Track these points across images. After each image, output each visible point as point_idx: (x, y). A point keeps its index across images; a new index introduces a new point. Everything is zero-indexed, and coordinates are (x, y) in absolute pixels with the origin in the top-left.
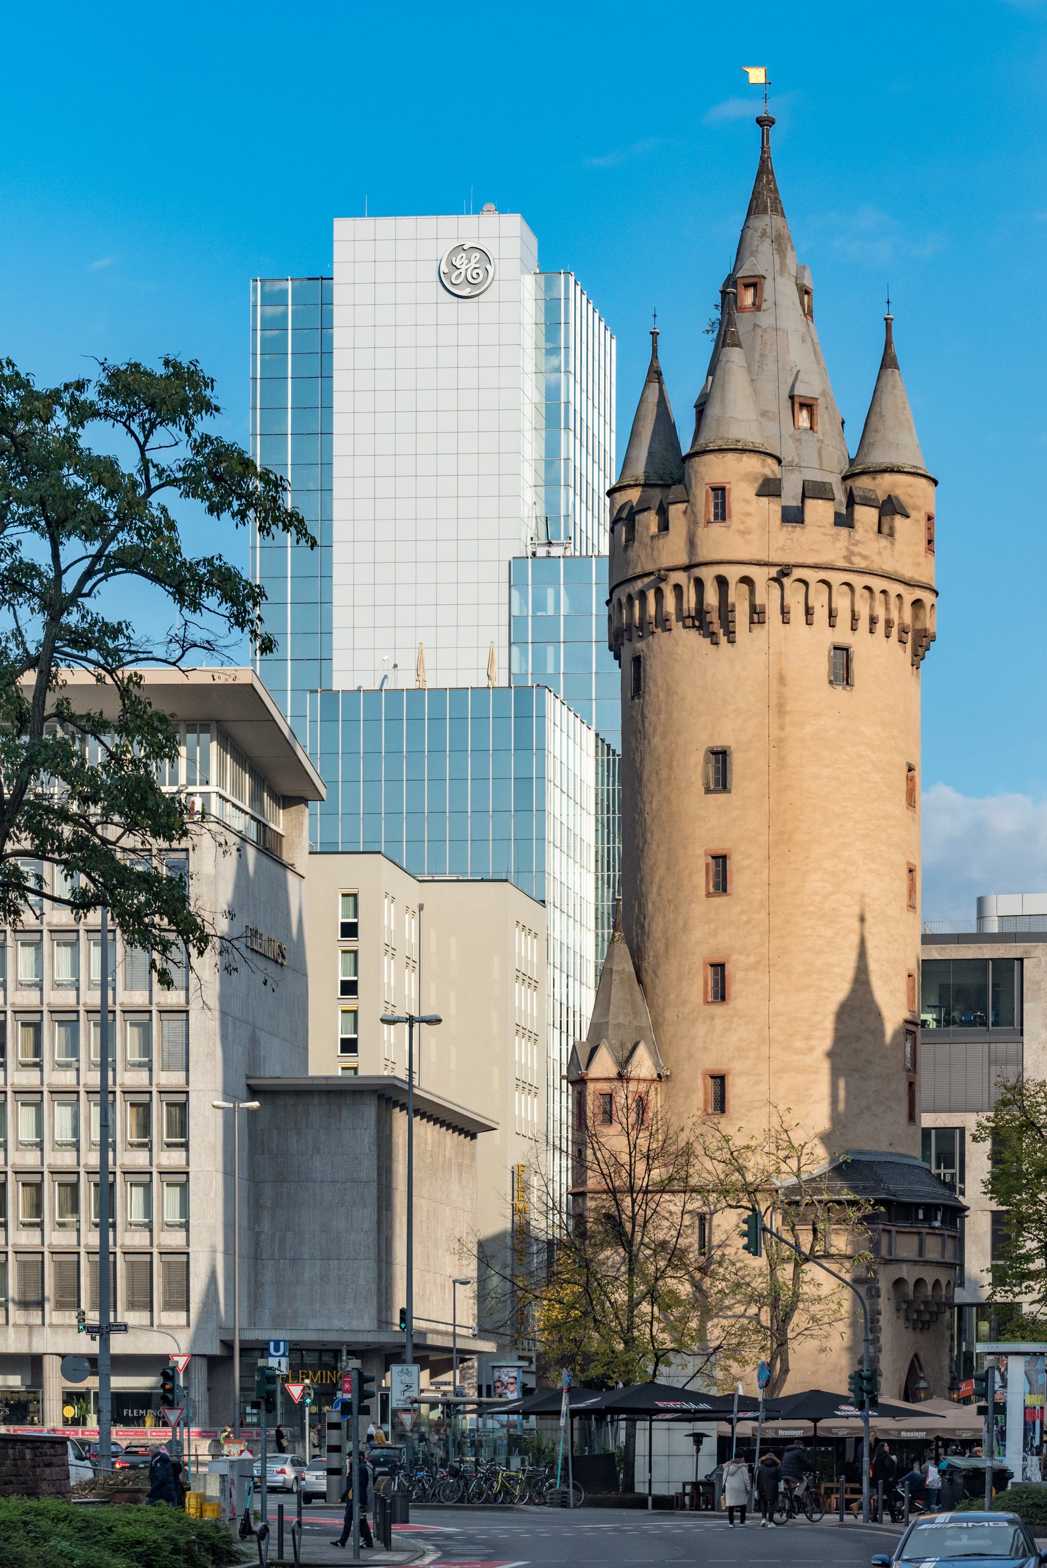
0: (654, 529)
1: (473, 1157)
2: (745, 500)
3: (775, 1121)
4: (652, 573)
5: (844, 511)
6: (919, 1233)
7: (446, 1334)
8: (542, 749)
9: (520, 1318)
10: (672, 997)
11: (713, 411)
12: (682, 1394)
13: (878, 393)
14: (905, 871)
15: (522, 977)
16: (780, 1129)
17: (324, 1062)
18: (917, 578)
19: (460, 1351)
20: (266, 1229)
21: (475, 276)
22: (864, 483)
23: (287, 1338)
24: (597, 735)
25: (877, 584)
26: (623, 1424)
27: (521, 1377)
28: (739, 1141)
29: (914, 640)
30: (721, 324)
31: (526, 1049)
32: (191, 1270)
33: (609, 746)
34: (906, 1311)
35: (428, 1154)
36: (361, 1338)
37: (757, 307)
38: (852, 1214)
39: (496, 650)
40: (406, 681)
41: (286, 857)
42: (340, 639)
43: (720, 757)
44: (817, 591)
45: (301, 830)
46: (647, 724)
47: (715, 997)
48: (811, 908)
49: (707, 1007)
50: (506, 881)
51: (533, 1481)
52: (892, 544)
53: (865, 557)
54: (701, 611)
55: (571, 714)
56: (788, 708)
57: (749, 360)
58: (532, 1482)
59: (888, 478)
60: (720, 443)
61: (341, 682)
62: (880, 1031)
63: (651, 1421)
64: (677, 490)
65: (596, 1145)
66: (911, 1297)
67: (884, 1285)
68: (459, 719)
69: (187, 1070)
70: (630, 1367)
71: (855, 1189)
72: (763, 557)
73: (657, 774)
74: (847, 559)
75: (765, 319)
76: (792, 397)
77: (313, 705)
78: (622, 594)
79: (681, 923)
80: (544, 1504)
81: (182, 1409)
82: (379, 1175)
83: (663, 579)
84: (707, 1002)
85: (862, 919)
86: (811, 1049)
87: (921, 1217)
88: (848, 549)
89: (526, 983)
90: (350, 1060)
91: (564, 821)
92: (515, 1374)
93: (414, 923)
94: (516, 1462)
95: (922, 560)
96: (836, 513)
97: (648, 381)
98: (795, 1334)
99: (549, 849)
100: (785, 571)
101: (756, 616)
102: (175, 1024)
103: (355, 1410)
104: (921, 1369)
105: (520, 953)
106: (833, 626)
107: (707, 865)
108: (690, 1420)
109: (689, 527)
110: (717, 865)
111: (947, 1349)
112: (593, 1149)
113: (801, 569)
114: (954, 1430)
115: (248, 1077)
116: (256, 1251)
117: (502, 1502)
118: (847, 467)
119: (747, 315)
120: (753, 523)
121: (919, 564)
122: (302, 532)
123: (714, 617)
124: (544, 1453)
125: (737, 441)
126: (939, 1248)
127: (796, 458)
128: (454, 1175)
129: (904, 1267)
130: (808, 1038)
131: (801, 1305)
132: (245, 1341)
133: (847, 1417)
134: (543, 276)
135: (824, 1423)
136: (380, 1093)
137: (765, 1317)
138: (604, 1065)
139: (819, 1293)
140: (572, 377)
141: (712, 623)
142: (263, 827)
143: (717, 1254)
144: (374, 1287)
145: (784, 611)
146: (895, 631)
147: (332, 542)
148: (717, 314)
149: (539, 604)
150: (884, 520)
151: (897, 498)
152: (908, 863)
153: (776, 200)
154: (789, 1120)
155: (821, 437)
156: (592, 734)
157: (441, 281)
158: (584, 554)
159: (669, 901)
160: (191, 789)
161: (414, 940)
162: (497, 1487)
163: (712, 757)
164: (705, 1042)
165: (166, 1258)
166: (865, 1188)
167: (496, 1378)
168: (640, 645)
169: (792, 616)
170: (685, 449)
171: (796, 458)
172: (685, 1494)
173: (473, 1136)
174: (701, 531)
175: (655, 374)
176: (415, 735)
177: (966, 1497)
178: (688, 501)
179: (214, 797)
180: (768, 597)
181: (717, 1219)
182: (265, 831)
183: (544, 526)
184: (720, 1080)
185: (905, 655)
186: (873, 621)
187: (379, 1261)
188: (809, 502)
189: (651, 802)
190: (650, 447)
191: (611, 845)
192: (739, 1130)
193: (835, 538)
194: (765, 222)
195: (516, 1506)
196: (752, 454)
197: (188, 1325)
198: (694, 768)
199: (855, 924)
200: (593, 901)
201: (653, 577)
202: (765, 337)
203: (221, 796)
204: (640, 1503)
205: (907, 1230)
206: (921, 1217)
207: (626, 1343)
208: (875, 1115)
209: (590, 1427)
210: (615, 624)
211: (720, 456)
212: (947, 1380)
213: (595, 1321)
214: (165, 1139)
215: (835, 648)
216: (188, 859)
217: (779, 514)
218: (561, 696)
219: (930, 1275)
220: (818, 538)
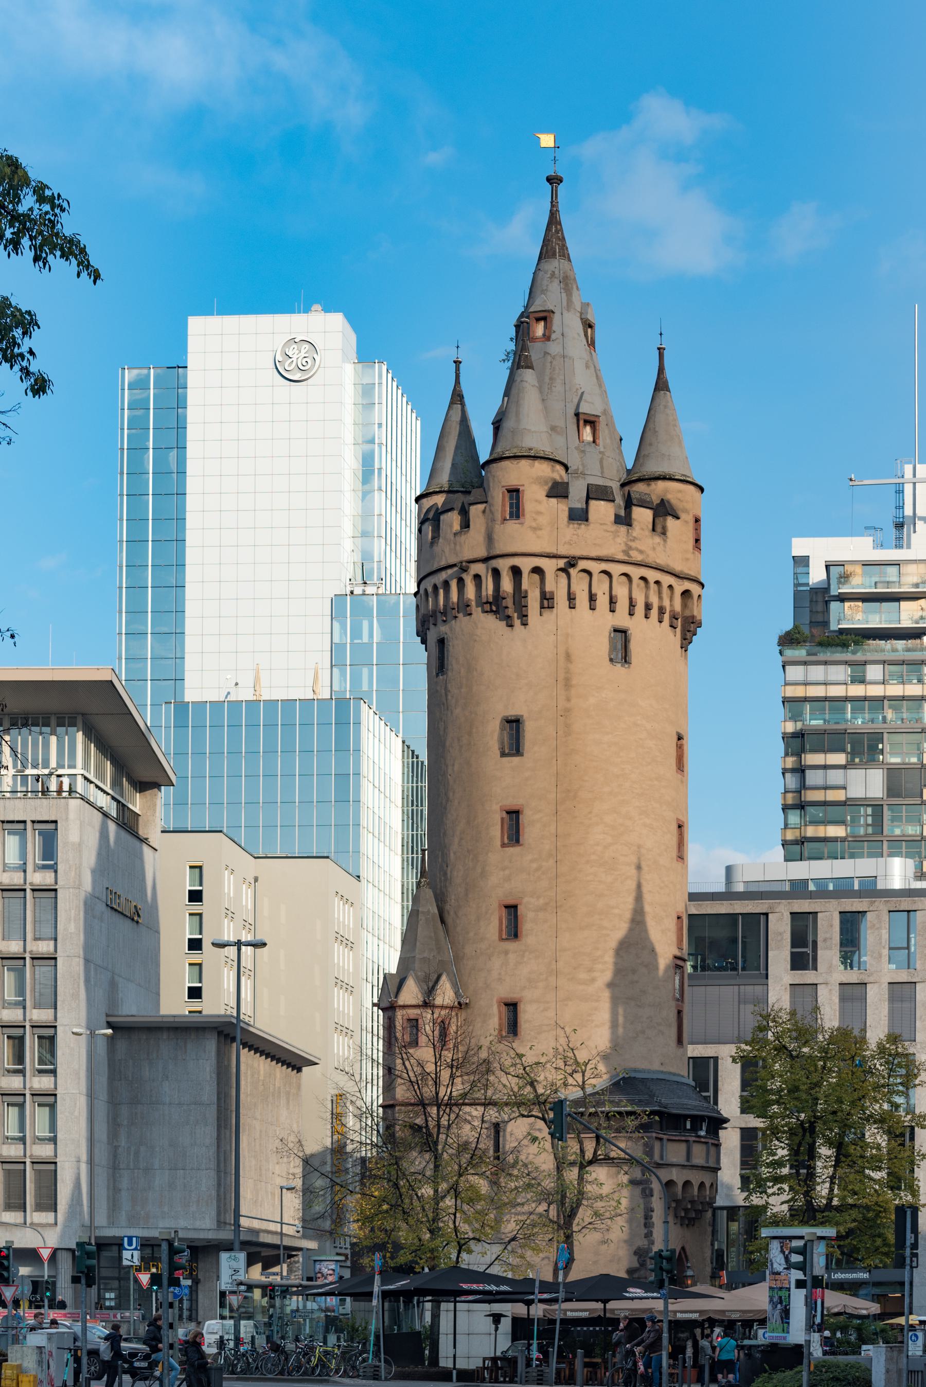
0: (457, 527)
1: (299, 1087)
2: (536, 501)
3: (563, 1041)
4: (454, 565)
5: (622, 513)
6: (687, 1141)
7: (275, 1233)
8: (358, 750)
9: (338, 1215)
10: (471, 934)
11: (508, 424)
12: (484, 1277)
13: (652, 412)
14: (675, 826)
15: (340, 938)
16: (566, 1048)
17: (174, 1004)
18: (686, 571)
19: (287, 1248)
20: (123, 1144)
21: (304, 364)
22: (640, 487)
23: (140, 1235)
24: (404, 742)
25: (652, 575)
26: (428, 1305)
27: (338, 1270)
28: (529, 1059)
29: (683, 626)
30: (515, 354)
31: (344, 955)
32: (58, 1177)
33: (413, 752)
34: (675, 1209)
35: (261, 1083)
36: (202, 1236)
37: (547, 337)
38: (631, 1123)
39: (320, 671)
40: (245, 694)
41: (142, 832)
42: (190, 662)
43: (514, 724)
44: (599, 581)
45: (155, 811)
46: (449, 697)
47: (509, 935)
48: (593, 857)
49: (502, 943)
50: (327, 857)
51: (348, 1356)
52: (665, 541)
53: (641, 552)
54: (498, 596)
55: (382, 723)
56: (574, 682)
57: (540, 380)
58: (346, 1356)
59: (661, 484)
60: (515, 451)
61: (190, 696)
62: (652, 965)
63: (455, 1302)
64: (476, 493)
65: (405, 1056)
66: (680, 1196)
67: (656, 1186)
68: (288, 726)
69: (56, 1008)
70: (435, 1254)
71: (632, 1102)
72: (552, 550)
73: (459, 740)
74: (626, 552)
75: (554, 348)
76: (577, 415)
77: (167, 715)
78: (428, 584)
79: (479, 871)
80: (358, 1376)
81: (17, 1286)
82: (219, 1099)
83: (464, 570)
84: (501, 939)
85: (639, 868)
86: (593, 980)
87: (688, 1127)
88: (626, 545)
89: (344, 943)
90: (195, 1005)
91: (376, 860)
92: (333, 1267)
93: (250, 892)
94: (332, 1339)
95: (690, 556)
96: (616, 515)
97: (452, 403)
98: (580, 1227)
99: (363, 833)
100: (572, 562)
101: (546, 602)
102: (44, 970)
103: (165, 1281)
104: (687, 1260)
105: (338, 919)
106: (613, 611)
107: (502, 819)
108: (489, 1302)
109: (487, 524)
110: (511, 819)
111: (709, 1243)
112: (402, 1059)
113: (585, 561)
114: (723, 1312)
115: (107, 1015)
116: (114, 1162)
117: (319, 1375)
118: (625, 476)
119: (538, 345)
120: (543, 520)
121: (687, 559)
122: (85, 264)
123: (509, 602)
124: (357, 1330)
125: (531, 449)
126: (704, 1154)
127: (580, 467)
128: (283, 1101)
129: (674, 1170)
130: (590, 970)
131: (585, 1202)
132: (100, 1237)
133: (632, 1299)
134: (360, 365)
135: (611, 1305)
136: (220, 1029)
137: (553, 1213)
138: (411, 993)
139: (601, 1192)
140: (384, 448)
141: (507, 608)
142: (121, 806)
143: (511, 1159)
144: (214, 1193)
145: (571, 598)
146: (666, 617)
147: (185, 583)
148: (512, 346)
149: (356, 632)
150: (657, 521)
151: (668, 502)
152: (678, 819)
153: (564, 247)
154: (575, 1041)
155: (602, 450)
156: (400, 741)
157: (277, 368)
158: (393, 592)
159: (468, 851)
160: (60, 772)
161: (250, 906)
162: (314, 1361)
163: (507, 725)
164: (500, 974)
165: (37, 1167)
166: (640, 1101)
167: (317, 1270)
168: (443, 629)
169: (578, 602)
170: (484, 457)
171: (580, 467)
172: (484, 1368)
173: (299, 1070)
174: (498, 528)
175: (457, 397)
176: (252, 738)
177: (765, 1371)
178: (486, 502)
179: (80, 779)
180: (556, 585)
181: (510, 1127)
182: (123, 810)
183: (360, 571)
184: (512, 1007)
185: (675, 639)
186: (648, 607)
187: (219, 1171)
188: (593, 504)
189: (453, 765)
190: (453, 459)
191: (420, 808)
192: (531, 1048)
193: (616, 534)
194: (553, 265)
195: (331, 1379)
196: (543, 461)
197: (56, 1224)
198: (491, 734)
199: (633, 871)
200: (400, 878)
201: (455, 569)
202: (554, 363)
203: (86, 778)
204: (445, 1376)
205: (677, 1138)
206: (688, 1127)
207: (431, 1232)
208: (648, 1038)
209: (399, 1308)
210: (422, 611)
211: (515, 462)
212: (708, 1270)
213: (404, 1213)
214: (37, 1066)
215: (616, 631)
216: (56, 829)
217: (566, 513)
218: (374, 707)
219: (696, 1178)
220: (600, 534)
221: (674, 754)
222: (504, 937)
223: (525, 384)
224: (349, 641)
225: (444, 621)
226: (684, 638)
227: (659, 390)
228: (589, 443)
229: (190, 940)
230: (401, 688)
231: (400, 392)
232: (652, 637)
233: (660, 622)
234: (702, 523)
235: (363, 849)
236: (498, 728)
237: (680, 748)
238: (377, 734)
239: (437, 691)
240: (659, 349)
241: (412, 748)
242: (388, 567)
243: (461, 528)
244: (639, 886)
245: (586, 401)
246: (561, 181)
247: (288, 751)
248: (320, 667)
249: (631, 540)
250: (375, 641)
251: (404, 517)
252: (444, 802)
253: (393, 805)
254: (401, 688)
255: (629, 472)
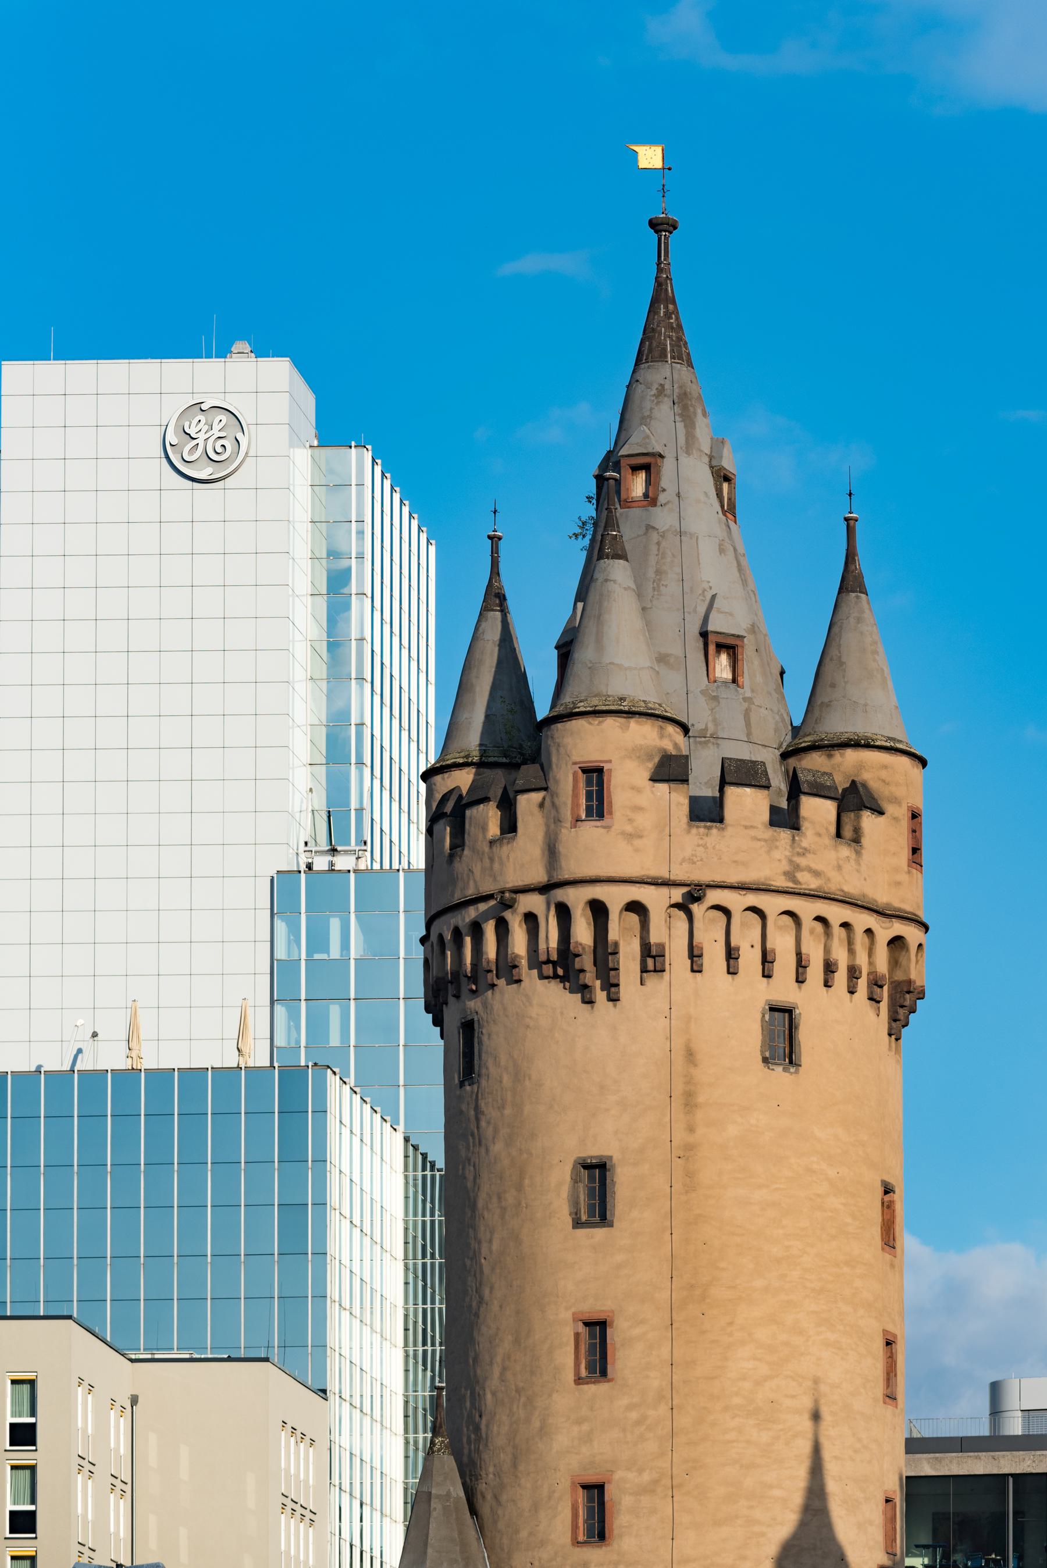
0: (494, 829)
2: (633, 788)
5: (784, 805)
8: (321, 1161)
10: (524, 1534)
11: (584, 655)
13: (835, 629)
14: (879, 1344)
15: (290, 1505)
18: (897, 904)
21: (219, 449)
22: (815, 761)
24: (407, 1140)
25: (836, 914)
29: (890, 997)
30: (596, 525)
33: (425, 1156)
37: (650, 499)
39: (250, 1012)
40: (110, 1057)
43: (597, 1173)
46: (483, 1124)
47: (590, 1534)
48: (737, 1400)
49: (578, 1550)
52: (858, 853)
53: (817, 874)
56: (701, 1099)
59: (851, 756)
60: (595, 701)
64: (528, 772)
68: (193, 1116)
72: (662, 873)
73: (499, 1198)
74: (790, 875)
75: (663, 518)
76: (704, 635)
78: (445, 927)
83: (508, 905)
84: (576, 1543)
85: (816, 1417)
88: (791, 862)
89: (297, 1514)
91: (356, 1360)
93: (124, 1424)
95: (903, 877)
97: (485, 609)
99: (333, 1311)
100: (694, 894)
101: (650, 962)
105: (288, 1470)
107: (577, 1336)
109: (547, 826)
110: (592, 1336)
118: (789, 738)
119: (635, 512)
120: (645, 821)
121: (898, 884)
123: (586, 962)
127: (711, 726)
141: (583, 972)
145: (694, 955)
146: (862, 984)
148: (590, 510)
149: (318, 940)
151: (864, 785)
153: (680, 342)
155: (748, 694)
157: (167, 457)
158: (386, 866)
159: (518, 1391)
161: (124, 1449)
163: (585, 1173)
168: (473, 1004)
169: (706, 961)
170: (542, 711)
171: (711, 726)
174: (566, 834)
175: (495, 598)
176: (125, 1139)
178: (546, 789)
180: (669, 932)
183: (325, 825)
185: (878, 1021)
186: (829, 968)
188: (731, 792)
189: (490, 1241)
190: (488, 707)
193: (771, 845)
194: (660, 374)
196: (643, 719)
198: (556, 1189)
199: (807, 1424)
200: (400, 1390)
201: (492, 903)
202: (664, 544)
211: (595, 721)
215: (773, 1009)
218: (351, 1080)
220: (745, 844)
221: (878, 1219)
222: (581, 1538)
223: (611, 586)
224: (303, 956)
225: (473, 992)
226: (894, 1018)
227: (848, 591)
228: (725, 683)
229: (12, 1514)
230: (402, 1042)
231: (397, 497)
232: (838, 1021)
233: (852, 992)
234: (924, 819)
235: (332, 1340)
236: (568, 1178)
237: (888, 1208)
238: (357, 1130)
239: (461, 1112)
240: (846, 519)
241: (422, 1150)
242: (377, 733)
243: (503, 832)
244: (817, 1450)
245: (719, 611)
246: (675, 228)
247: (192, 1162)
248: (250, 1003)
249: (799, 854)
250: (353, 955)
251: (405, 725)
252: (474, 1304)
253: (387, 1257)
254: (402, 1042)
255: (796, 731)
